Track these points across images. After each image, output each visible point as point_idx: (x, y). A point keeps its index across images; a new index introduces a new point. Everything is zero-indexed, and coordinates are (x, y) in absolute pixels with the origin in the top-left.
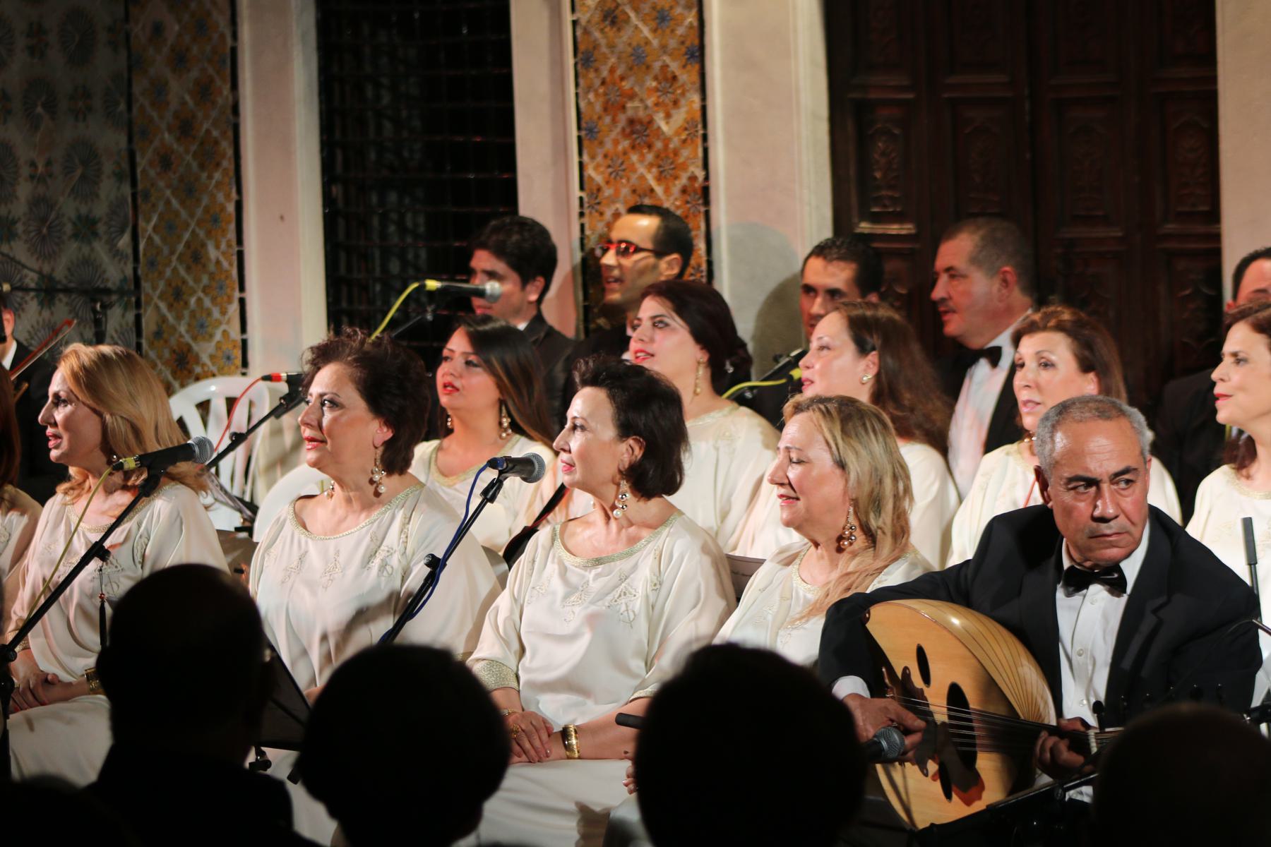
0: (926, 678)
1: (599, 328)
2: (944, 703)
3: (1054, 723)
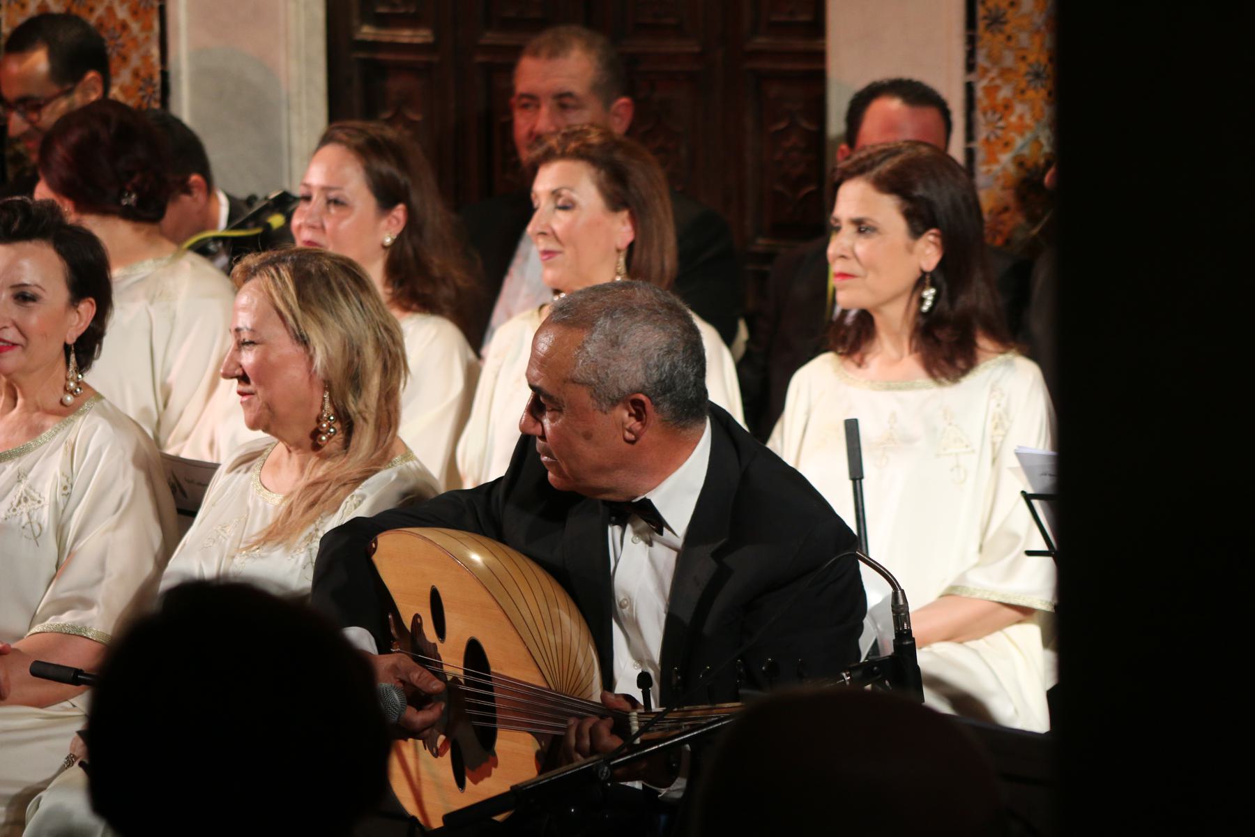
0: (441, 631)
1: (782, 558)
2: (461, 663)
3: (597, 698)
